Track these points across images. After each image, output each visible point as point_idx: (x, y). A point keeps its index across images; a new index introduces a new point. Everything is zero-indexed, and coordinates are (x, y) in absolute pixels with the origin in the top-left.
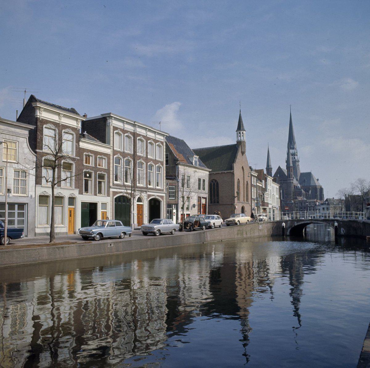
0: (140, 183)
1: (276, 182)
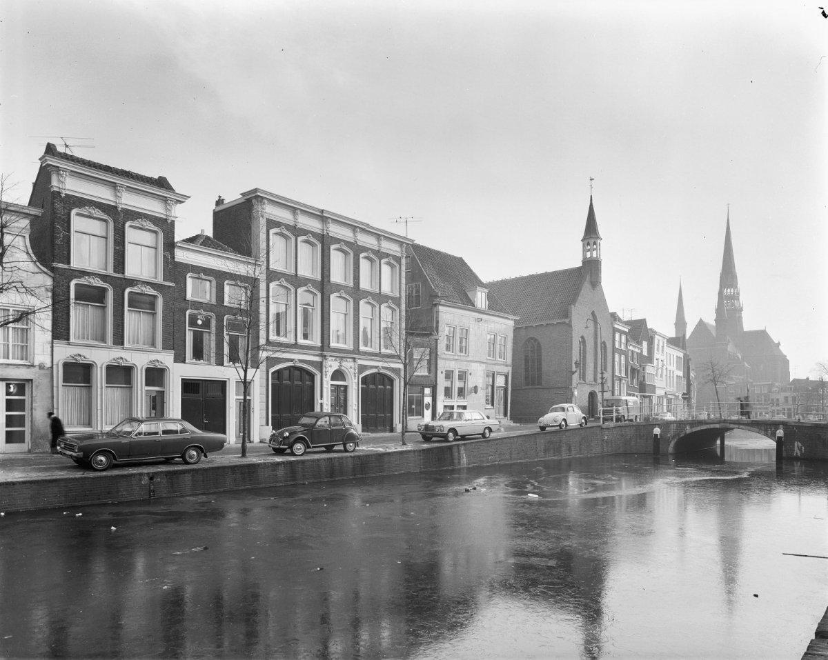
0: (281, 334)
1: (678, 346)
